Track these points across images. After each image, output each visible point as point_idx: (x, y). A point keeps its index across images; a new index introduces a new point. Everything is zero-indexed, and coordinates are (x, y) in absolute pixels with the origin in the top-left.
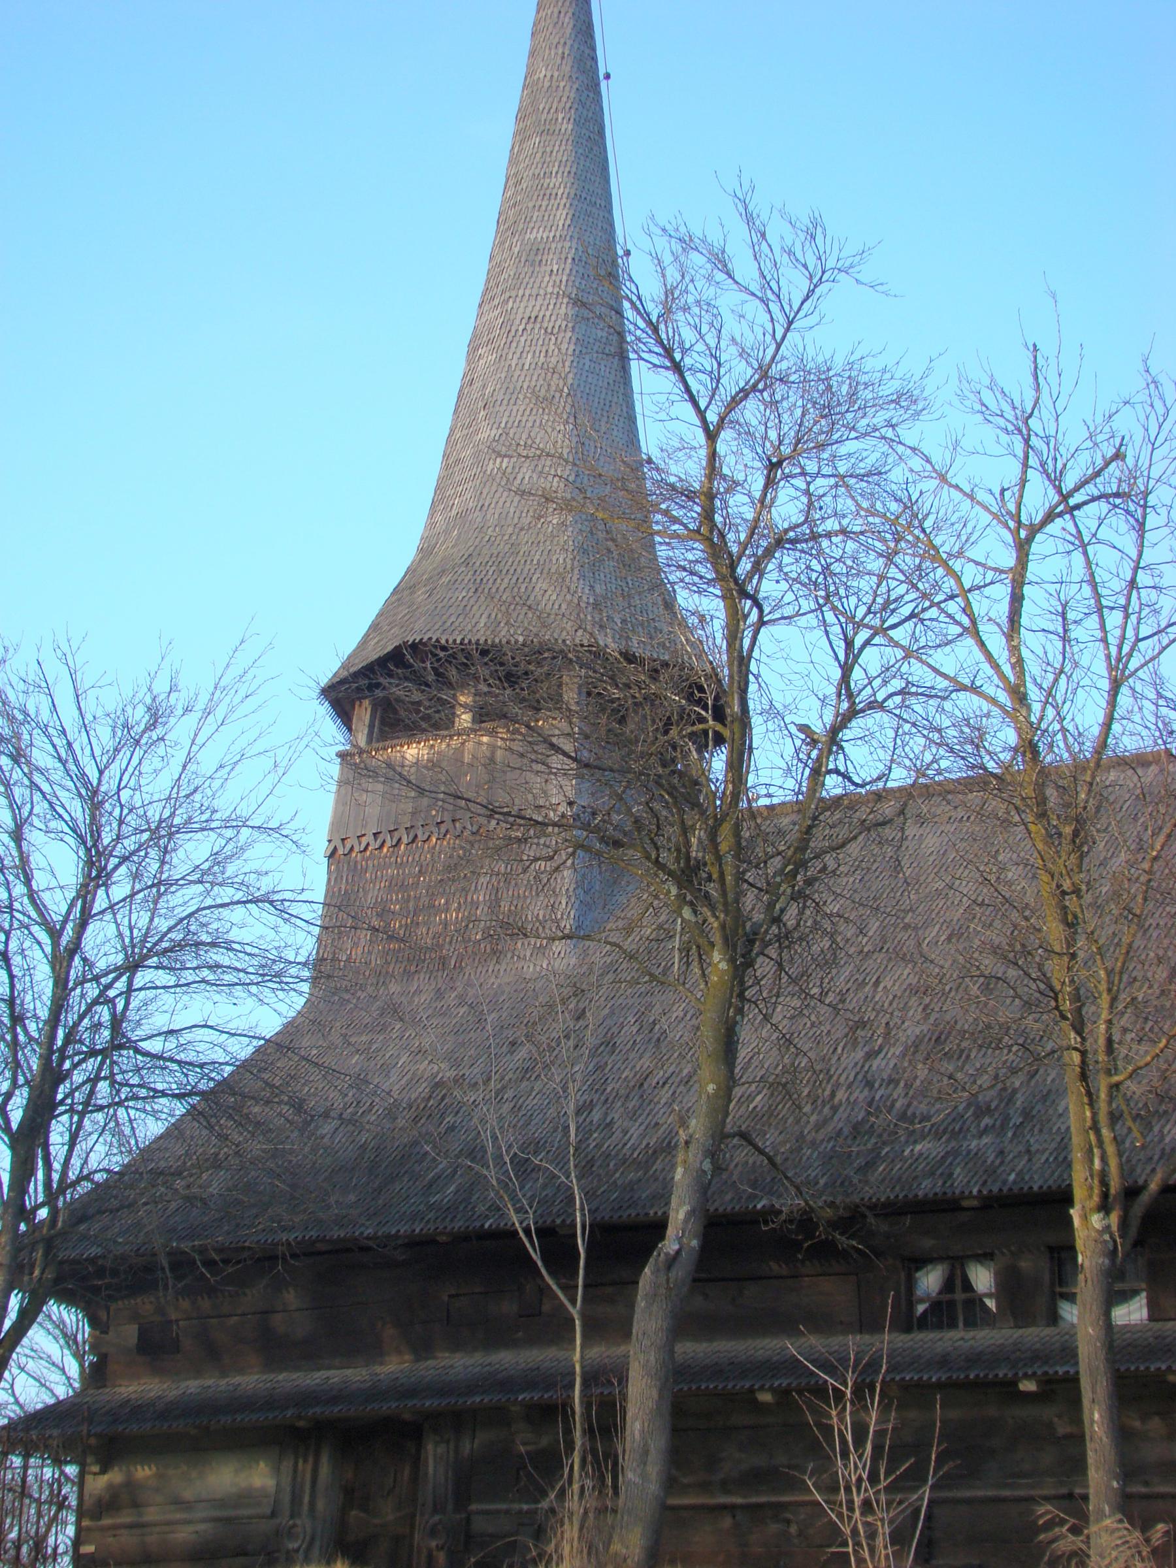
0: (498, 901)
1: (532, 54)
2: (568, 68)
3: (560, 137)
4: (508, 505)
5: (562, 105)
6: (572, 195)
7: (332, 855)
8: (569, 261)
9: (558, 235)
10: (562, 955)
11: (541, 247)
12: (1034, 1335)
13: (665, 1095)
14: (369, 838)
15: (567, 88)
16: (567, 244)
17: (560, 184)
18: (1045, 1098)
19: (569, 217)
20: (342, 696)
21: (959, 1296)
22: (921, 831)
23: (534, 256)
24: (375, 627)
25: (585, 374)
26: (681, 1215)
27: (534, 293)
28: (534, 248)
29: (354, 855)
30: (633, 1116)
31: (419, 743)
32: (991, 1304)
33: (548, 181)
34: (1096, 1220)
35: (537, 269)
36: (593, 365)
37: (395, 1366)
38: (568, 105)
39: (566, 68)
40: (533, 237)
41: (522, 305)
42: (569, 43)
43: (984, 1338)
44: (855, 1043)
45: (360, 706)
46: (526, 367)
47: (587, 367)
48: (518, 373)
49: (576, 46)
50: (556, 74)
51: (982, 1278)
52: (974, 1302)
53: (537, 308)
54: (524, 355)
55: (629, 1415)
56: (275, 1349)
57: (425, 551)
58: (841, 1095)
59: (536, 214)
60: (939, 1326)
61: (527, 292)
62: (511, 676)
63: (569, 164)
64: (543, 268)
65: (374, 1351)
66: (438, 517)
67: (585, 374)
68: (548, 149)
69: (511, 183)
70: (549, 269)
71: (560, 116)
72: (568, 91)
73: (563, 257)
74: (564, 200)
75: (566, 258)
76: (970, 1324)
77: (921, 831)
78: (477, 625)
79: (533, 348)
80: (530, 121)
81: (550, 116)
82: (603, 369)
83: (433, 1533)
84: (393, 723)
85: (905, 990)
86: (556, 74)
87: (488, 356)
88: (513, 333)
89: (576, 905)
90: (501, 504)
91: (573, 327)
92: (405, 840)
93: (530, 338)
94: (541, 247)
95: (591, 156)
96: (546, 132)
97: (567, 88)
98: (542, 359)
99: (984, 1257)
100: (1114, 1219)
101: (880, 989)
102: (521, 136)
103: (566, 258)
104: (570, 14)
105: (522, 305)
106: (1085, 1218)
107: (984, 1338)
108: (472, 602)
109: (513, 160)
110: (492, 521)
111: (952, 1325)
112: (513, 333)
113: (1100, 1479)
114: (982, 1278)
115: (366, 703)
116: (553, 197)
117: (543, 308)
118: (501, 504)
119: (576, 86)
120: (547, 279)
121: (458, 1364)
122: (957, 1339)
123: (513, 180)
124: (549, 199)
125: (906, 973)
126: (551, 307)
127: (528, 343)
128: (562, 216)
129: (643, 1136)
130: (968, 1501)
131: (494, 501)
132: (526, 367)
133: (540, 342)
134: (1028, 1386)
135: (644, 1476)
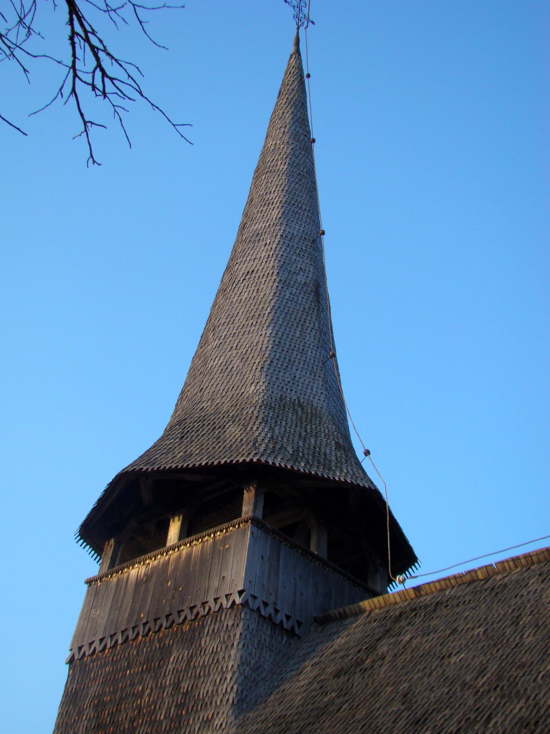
0: (179, 683)
2: (287, 138)
3: (278, 173)
4: (219, 385)
5: (281, 157)
6: (284, 202)
7: (71, 661)
8: (279, 236)
9: (272, 224)
10: (224, 726)
11: (260, 233)
14: (96, 644)
15: (286, 148)
16: (278, 228)
19: (280, 213)
22: (542, 586)
25: (285, 301)
27: (253, 258)
28: (256, 234)
29: (85, 659)
31: (140, 563)
33: (268, 196)
35: (256, 244)
36: (292, 296)
38: (285, 156)
39: (286, 139)
40: (255, 228)
41: (244, 266)
42: (288, 126)
45: (108, 545)
46: (243, 301)
47: (287, 297)
48: (237, 304)
49: (293, 128)
50: (278, 142)
53: (255, 265)
54: (243, 294)
59: (259, 215)
61: (248, 259)
63: (283, 186)
64: (261, 243)
67: (285, 301)
68: (270, 181)
69: (248, 205)
70: (264, 242)
71: (279, 163)
73: (274, 235)
74: (278, 204)
75: (276, 235)
77: (542, 586)
79: (249, 289)
81: (273, 164)
82: (300, 299)
85: (516, 724)
86: (278, 142)
88: (236, 283)
89: (240, 680)
90: (215, 385)
91: (278, 273)
92: (120, 642)
93: (247, 284)
94: (260, 233)
95: (299, 183)
97: (286, 148)
98: (255, 294)
101: (491, 725)
103: (276, 235)
104: (290, 112)
105: (244, 266)
108: (176, 445)
110: (206, 397)
112: (236, 283)
115: (112, 541)
116: (271, 204)
117: (258, 265)
118: (215, 385)
119: (290, 147)
120: (263, 248)
124: (268, 206)
125: (518, 707)
126: (263, 264)
127: (246, 286)
128: (275, 213)
131: (211, 384)
132: (243, 301)
133: (254, 284)
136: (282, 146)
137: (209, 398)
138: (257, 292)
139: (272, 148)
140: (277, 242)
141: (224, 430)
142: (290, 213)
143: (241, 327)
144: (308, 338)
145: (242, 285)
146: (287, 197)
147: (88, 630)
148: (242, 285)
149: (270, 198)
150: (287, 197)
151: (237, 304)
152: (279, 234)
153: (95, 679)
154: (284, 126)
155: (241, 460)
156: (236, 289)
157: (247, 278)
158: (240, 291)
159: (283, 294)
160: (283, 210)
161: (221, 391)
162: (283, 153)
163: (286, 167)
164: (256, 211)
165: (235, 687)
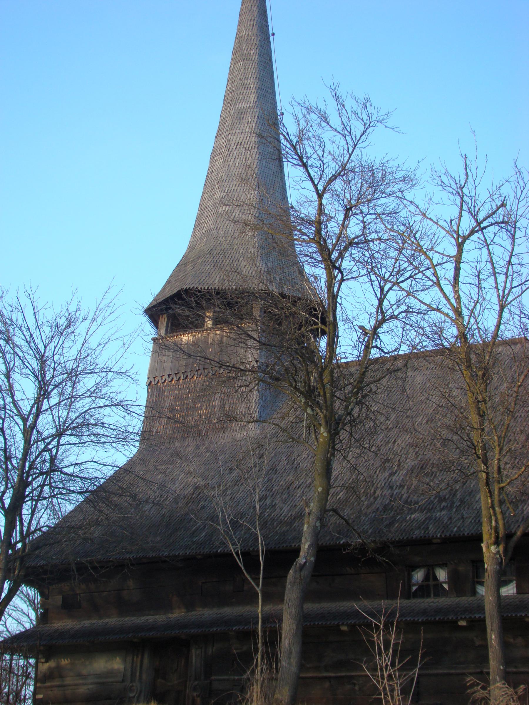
0: (224, 405)
1: (239, 24)
2: (256, 31)
4: (228, 227)
6: (257, 88)
7: (149, 385)
8: (256, 117)
9: (251, 106)
10: (253, 429)
12: (465, 600)
13: (299, 492)
15: (255, 40)
16: (255, 110)
17: (252, 82)
18: (470, 494)
19: (256, 97)
20: (154, 313)
21: (432, 583)
23: (240, 115)
24: (169, 282)
25: (263, 168)
26: (306, 546)
27: (240, 132)
28: (240, 112)
29: (159, 384)
30: (285, 502)
31: (189, 334)
32: (446, 586)
34: (493, 549)
35: (242, 121)
37: (177, 615)
38: (256, 47)
39: (255, 31)
41: (235, 137)
42: (256, 19)
43: (443, 601)
44: (385, 469)
46: (237, 165)
47: (264, 165)
48: (233, 167)
51: (442, 575)
52: (438, 585)
53: (242, 138)
54: (236, 160)
55: (283, 636)
56: (124, 607)
57: (191, 248)
58: (378, 492)
59: (241, 96)
60: (422, 596)
61: (237, 131)
62: (230, 304)
63: (256, 74)
64: (244, 121)
65: (168, 607)
66: (197, 233)
68: (247, 67)
70: (247, 121)
71: (252, 52)
72: (255, 41)
73: (253, 116)
74: (254, 90)
76: (436, 595)
78: (215, 281)
79: (240, 156)
80: (238, 55)
81: (247, 52)
83: (195, 689)
84: (177, 325)
85: (407, 445)
86: (250, 33)
87: (220, 160)
89: (259, 407)
90: (225, 226)
93: (238, 152)
96: (246, 59)
97: (255, 40)
99: (442, 565)
100: (501, 548)
101: (396, 445)
102: (234, 61)
103: (255, 116)
105: (235, 137)
106: (488, 547)
107: (443, 601)
109: (231, 72)
111: (428, 596)
112: (231, 150)
113: (495, 665)
114: (442, 575)
117: (244, 139)
121: (206, 613)
122: (430, 602)
123: (231, 81)
124: (247, 90)
125: (407, 437)
126: (248, 138)
128: (253, 97)
129: (289, 511)
130: (436, 675)
131: (222, 225)
133: (243, 154)
134: (462, 623)
135: (290, 664)
136: (253, 38)
137: (223, 235)
138: (246, 160)
139: (246, 38)
140: (255, 122)
141: (239, 263)
142: (262, 97)
143: (237, 185)
144: (277, 195)
145: (235, 152)
146: (259, 84)
147: (158, 368)
148: (235, 152)
149: (248, 83)
150: (259, 84)
151: (233, 167)
152: (256, 115)
153: (168, 396)
154: (253, 18)
155: (448, 535)
156: (231, 155)
157: (238, 147)
158: (234, 157)
159: (262, 163)
160: (257, 95)
161: (230, 231)
162: (254, 45)
163: (257, 57)
164: (239, 92)
165: (257, 411)
